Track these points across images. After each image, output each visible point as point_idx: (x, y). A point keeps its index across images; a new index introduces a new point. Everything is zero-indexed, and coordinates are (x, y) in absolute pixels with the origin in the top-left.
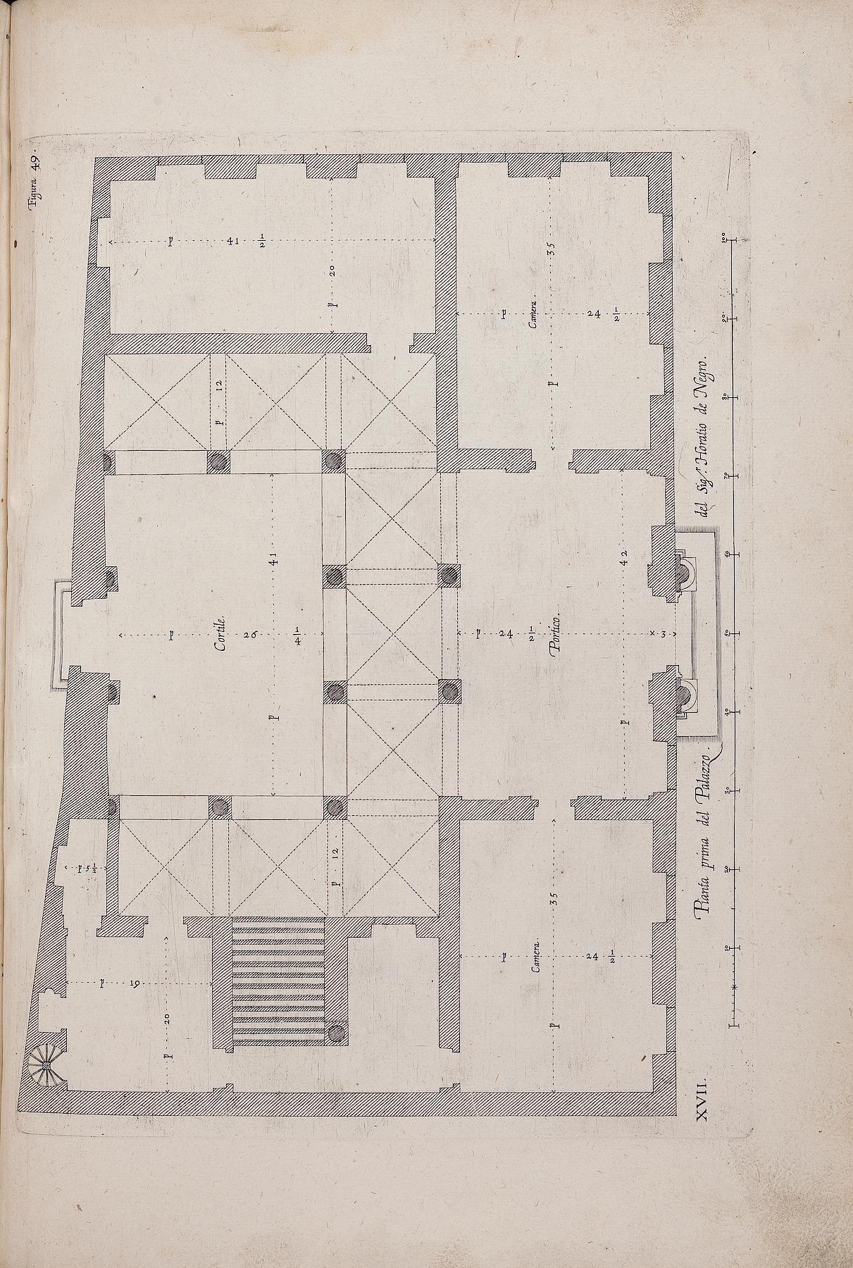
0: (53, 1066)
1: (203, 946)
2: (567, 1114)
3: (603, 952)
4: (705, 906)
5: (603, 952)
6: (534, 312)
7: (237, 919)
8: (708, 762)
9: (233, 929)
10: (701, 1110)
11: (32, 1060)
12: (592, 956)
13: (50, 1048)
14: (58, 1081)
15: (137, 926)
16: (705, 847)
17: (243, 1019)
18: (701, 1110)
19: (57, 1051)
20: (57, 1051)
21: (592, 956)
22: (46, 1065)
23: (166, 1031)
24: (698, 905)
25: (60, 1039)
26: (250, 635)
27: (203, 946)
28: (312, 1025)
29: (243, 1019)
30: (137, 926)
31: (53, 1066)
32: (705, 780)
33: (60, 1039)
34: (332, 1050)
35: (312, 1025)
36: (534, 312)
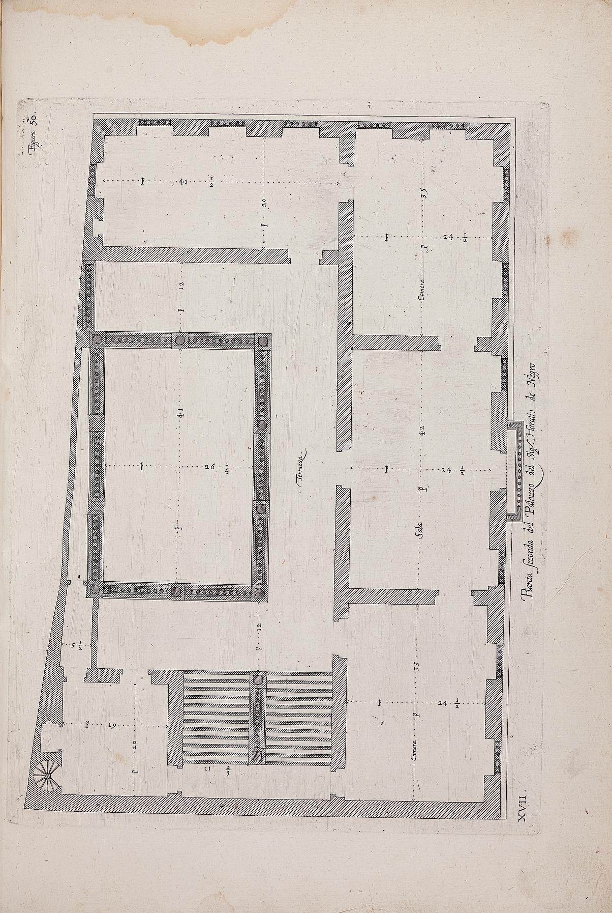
0: (53, 776)
1: (162, 691)
2: (422, 817)
3: (452, 701)
4: (529, 593)
5: (452, 701)
6: (415, 749)
7: (186, 672)
8: (533, 488)
9: (184, 704)
10: (522, 813)
11: (36, 772)
12: (446, 469)
13: (50, 763)
14: (56, 787)
15: (115, 676)
16: (530, 580)
17: (190, 721)
18: (522, 813)
19: (55, 765)
20: (55, 765)
21: (446, 469)
22: (47, 776)
23: (149, 466)
24: (523, 592)
25: (57, 757)
26: (210, 467)
27: (162, 691)
28: (239, 742)
29: (190, 721)
30: (115, 676)
31: (53, 776)
32: (531, 501)
33: (57, 757)
34: (253, 768)
35: (239, 742)
36: (415, 749)
